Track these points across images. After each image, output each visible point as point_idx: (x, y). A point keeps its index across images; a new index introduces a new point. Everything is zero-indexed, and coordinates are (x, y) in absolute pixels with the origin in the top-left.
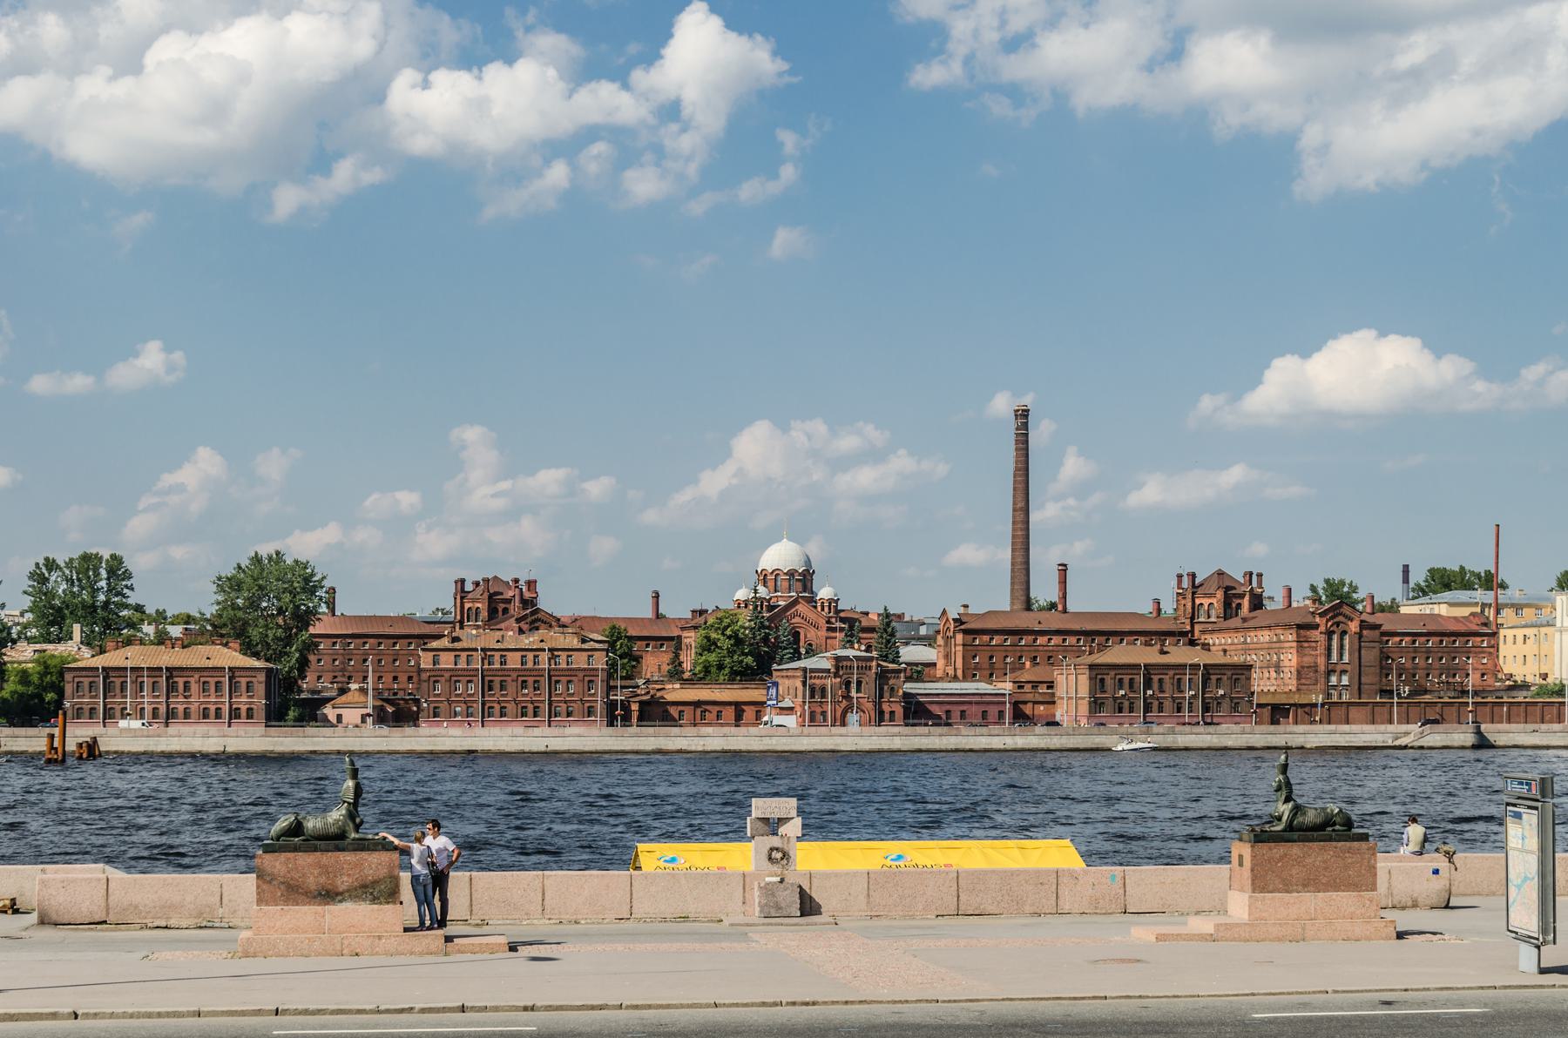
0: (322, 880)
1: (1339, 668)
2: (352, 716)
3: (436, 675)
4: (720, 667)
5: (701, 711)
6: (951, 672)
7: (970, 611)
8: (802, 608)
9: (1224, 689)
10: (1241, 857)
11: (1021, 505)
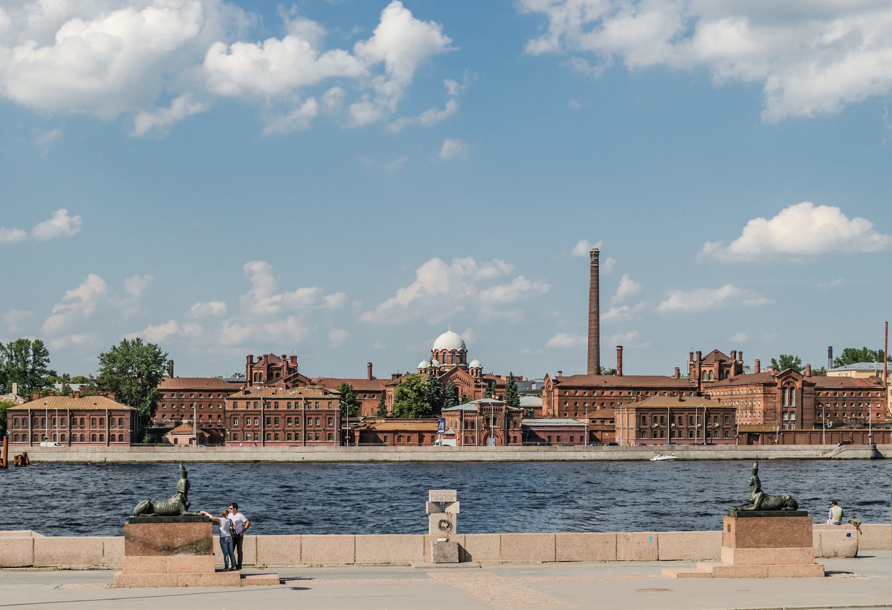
0: (165, 540)
1: (789, 410)
2: (183, 439)
3: (235, 414)
4: (410, 409)
6: (551, 412)
7: (563, 375)
8: (459, 373)
9: (718, 423)
10: (729, 526)
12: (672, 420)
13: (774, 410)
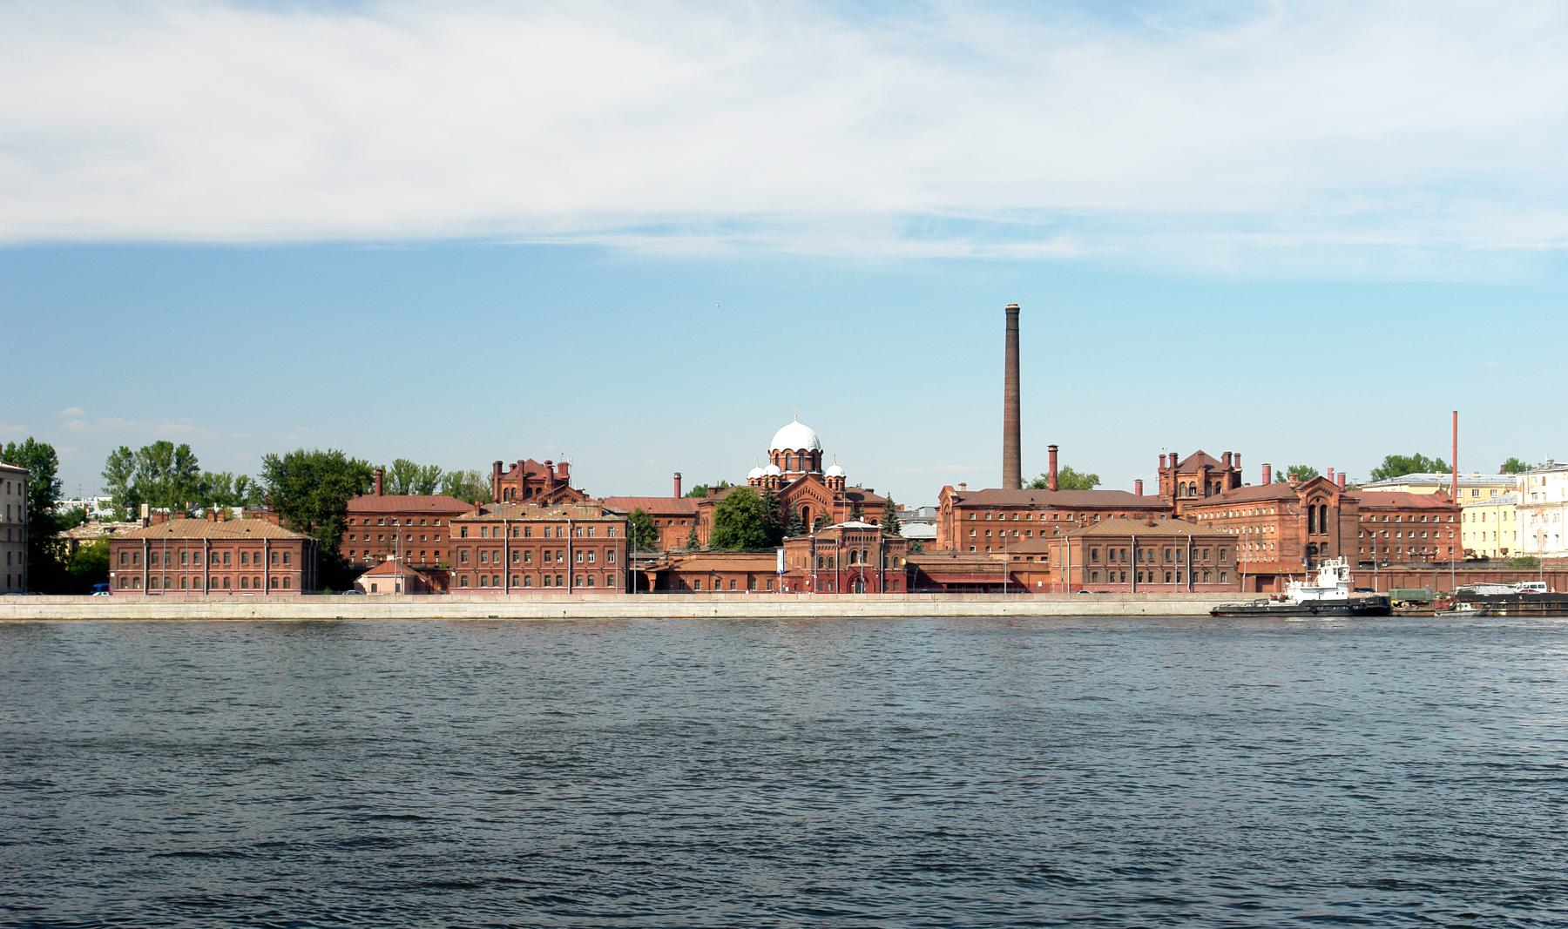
2: (387, 584)
4: (736, 537)
5: (716, 581)
6: (950, 545)
7: (968, 489)
8: (810, 484)
9: (1205, 559)
11: (1012, 394)
12: (1138, 553)
13: (1296, 540)
